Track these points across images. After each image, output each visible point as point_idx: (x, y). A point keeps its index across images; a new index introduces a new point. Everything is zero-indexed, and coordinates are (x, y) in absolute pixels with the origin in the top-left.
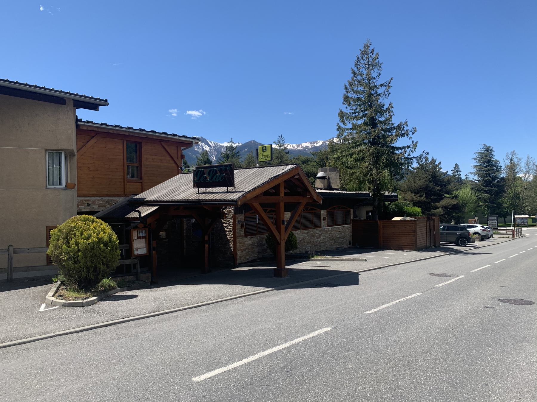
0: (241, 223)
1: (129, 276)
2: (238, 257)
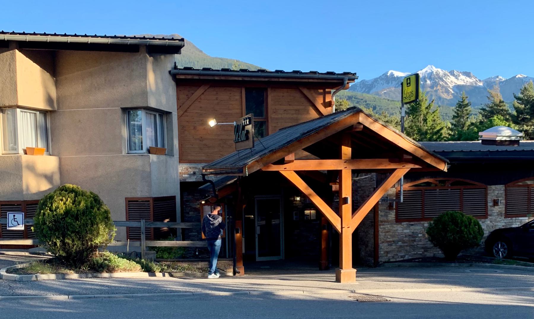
0: (388, 202)
2: (382, 252)
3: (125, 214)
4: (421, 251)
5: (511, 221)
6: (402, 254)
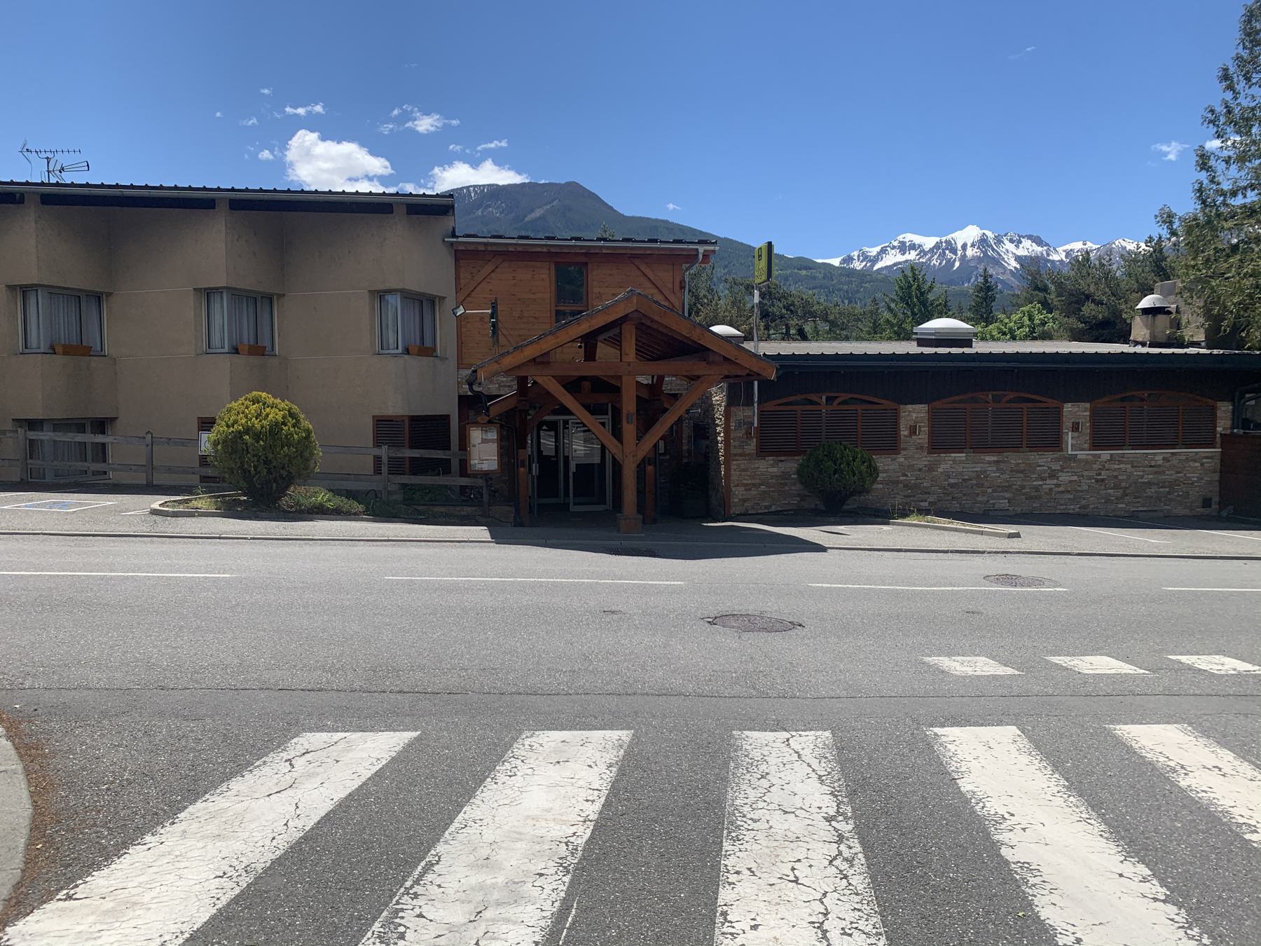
1: (468, 506)
2: (736, 500)
3: (372, 438)
4: (796, 500)
5: (938, 459)
6: (766, 504)
